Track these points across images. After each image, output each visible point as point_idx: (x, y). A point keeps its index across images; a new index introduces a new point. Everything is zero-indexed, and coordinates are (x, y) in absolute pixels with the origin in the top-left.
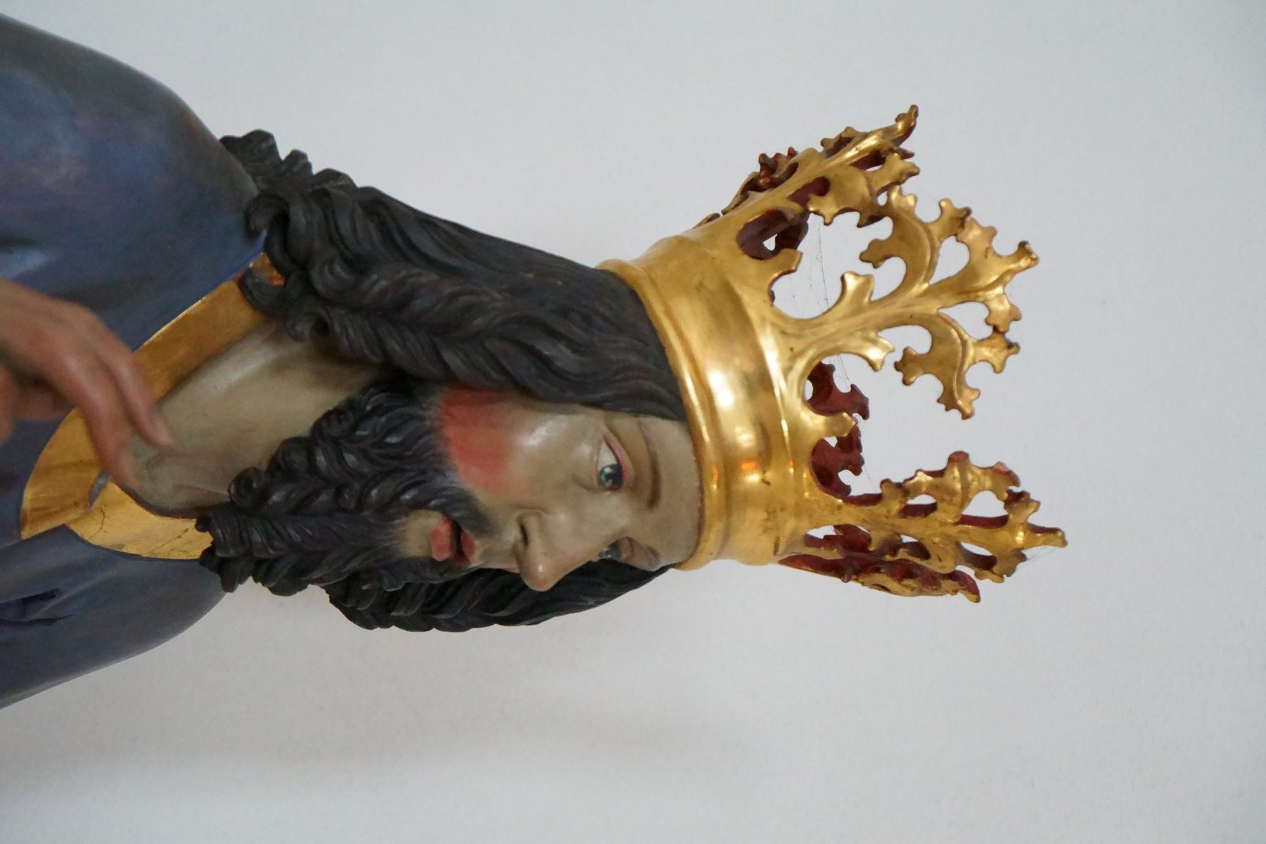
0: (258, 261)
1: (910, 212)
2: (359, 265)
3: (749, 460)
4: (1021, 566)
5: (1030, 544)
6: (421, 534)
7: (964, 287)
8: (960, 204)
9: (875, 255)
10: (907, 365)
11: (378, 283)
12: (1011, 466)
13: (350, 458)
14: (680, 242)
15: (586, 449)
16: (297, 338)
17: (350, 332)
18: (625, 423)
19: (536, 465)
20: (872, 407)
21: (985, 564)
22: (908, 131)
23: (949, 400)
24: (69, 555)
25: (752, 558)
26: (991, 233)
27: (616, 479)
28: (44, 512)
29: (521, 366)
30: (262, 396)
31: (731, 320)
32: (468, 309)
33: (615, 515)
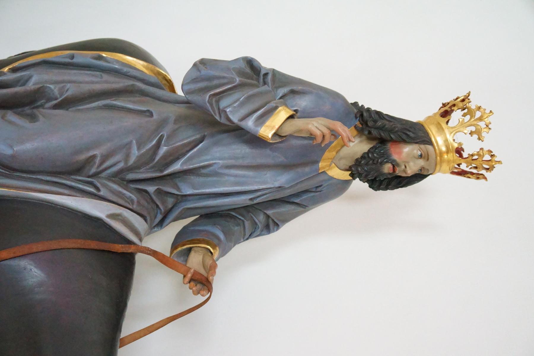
0: (357, 123)
1: (470, 107)
2: (375, 121)
3: (444, 153)
4: (494, 169)
5: (496, 164)
6: (387, 168)
7: (480, 119)
8: (479, 105)
9: (464, 115)
10: (471, 133)
11: (379, 123)
12: (491, 150)
13: (375, 155)
14: (429, 117)
15: (415, 151)
16: (364, 135)
17: (375, 133)
18: (422, 146)
19: (406, 156)
20: (465, 150)
21: (487, 169)
22: (469, 95)
23: (479, 139)
24: (326, 178)
25: (444, 172)
26: (485, 110)
27: (421, 156)
28: (323, 168)
29: (404, 137)
30: (359, 147)
31: (440, 129)
32: (395, 127)
33: (421, 163)
